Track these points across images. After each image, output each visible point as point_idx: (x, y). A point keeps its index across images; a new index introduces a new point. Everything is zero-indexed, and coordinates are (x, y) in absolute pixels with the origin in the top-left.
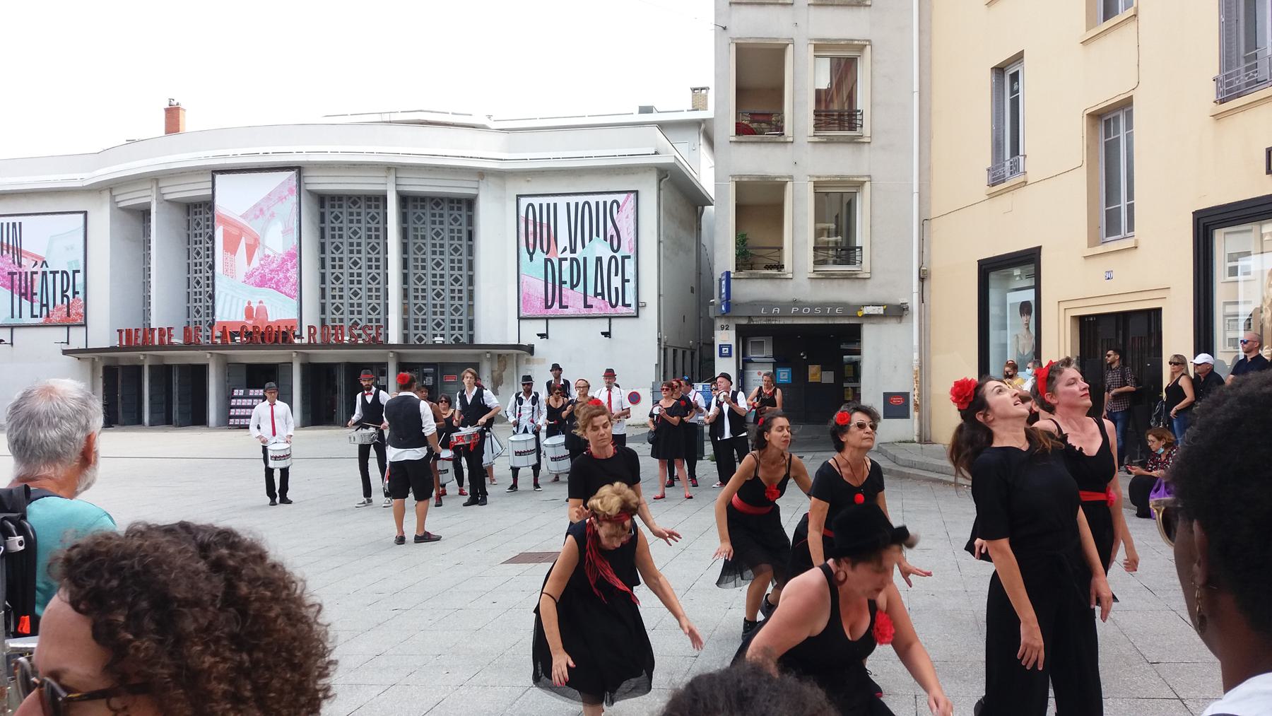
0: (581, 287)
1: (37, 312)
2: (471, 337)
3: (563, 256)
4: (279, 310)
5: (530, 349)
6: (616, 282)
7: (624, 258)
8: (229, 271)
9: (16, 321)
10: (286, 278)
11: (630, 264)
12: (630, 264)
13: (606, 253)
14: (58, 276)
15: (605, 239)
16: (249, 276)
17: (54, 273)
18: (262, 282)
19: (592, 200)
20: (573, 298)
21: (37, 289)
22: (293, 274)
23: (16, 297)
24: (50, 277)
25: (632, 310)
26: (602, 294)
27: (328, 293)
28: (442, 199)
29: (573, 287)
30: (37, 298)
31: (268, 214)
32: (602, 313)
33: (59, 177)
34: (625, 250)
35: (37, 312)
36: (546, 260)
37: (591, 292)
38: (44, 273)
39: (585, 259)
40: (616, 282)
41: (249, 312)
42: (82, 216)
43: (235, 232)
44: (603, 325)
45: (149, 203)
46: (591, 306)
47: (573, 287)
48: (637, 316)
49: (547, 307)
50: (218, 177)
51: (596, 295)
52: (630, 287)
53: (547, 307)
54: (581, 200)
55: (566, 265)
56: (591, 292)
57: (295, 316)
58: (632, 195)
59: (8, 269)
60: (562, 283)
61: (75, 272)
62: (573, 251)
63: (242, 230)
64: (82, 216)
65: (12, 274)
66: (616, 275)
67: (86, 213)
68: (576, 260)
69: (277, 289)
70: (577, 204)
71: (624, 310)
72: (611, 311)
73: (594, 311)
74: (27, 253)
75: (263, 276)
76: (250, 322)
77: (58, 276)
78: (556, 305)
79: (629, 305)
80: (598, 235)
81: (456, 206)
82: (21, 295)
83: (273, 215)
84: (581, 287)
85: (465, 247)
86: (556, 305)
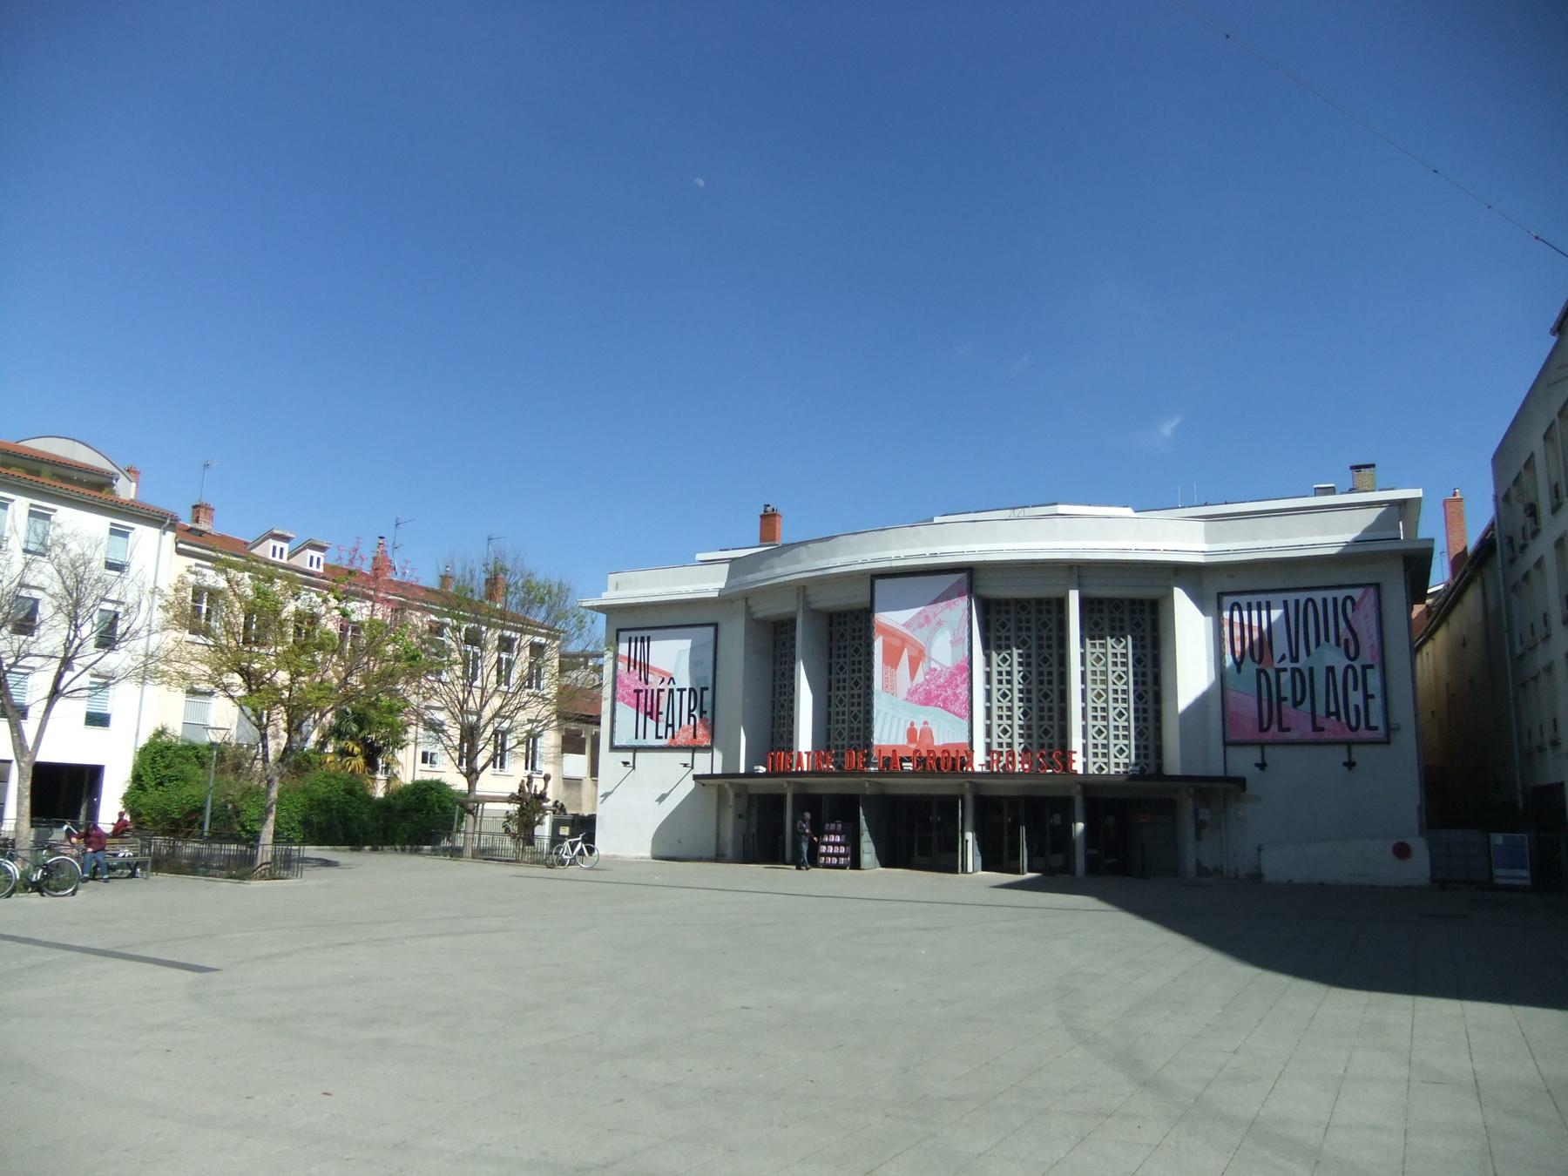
0: (1306, 706)
1: (662, 732)
2: (1160, 767)
3: (1282, 665)
4: (945, 732)
5: (1241, 783)
6: (1356, 698)
7: (1365, 668)
8: (890, 688)
9: (641, 742)
10: (955, 694)
11: (1374, 679)
12: (1374, 679)
13: (1340, 662)
14: (686, 694)
15: (1338, 644)
16: (912, 693)
17: (681, 690)
18: (928, 700)
19: (1318, 596)
20: (1298, 720)
21: (663, 708)
22: (963, 690)
23: (641, 716)
24: (677, 694)
25: (1381, 732)
26: (1337, 713)
27: (995, 712)
28: (1122, 601)
29: (1296, 704)
30: (663, 717)
31: (934, 622)
32: (1338, 737)
33: (691, 588)
34: (1366, 656)
35: (662, 732)
36: (1259, 672)
37: (1320, 711)
38: (671, 691)
39: (1311, 670)
40: (1356, 698)
41: (911, 733)
42: (711, 630)
43: (897, 643)
44: (1340, 754)
45: (795, 613)
46: (1322, 729)
47: (1296, 704)
48: (1388, 742)
49: (1262, 730)
50: (879, 583)
51: (1328, 714)
52: (1376, 704)
53: (1262, 730)
54: (1303, 597)
55: (1285, 677)
56: (1320, 711)
57: (966, 740)
58: (1372, 590)
59: (634, 687)
60: (1281, 699)
61: (703, 689)
62: (1295, 659)
63: (904, 640)
64: (711, 630)
65: (638, 691)
66: (1355, 688)
67: (716, 625)
68: (1299, 670)
69: (945, 708)
70: (1297, 602)
71: (1370, 735)
72: (1350, 735)
73: (1327, 736)
74: (655, 670)
75: (928, 693)
76: (913, 746)
77: (686, 694)
78: (1274, 727)
79: (1376, 728)
80: (1327, 639)
81: (1044, 608)
82: (646, 714)
83: (939, 623)
84: (1306, 706)
85: (1149, 656)
86: (1274, 727)
